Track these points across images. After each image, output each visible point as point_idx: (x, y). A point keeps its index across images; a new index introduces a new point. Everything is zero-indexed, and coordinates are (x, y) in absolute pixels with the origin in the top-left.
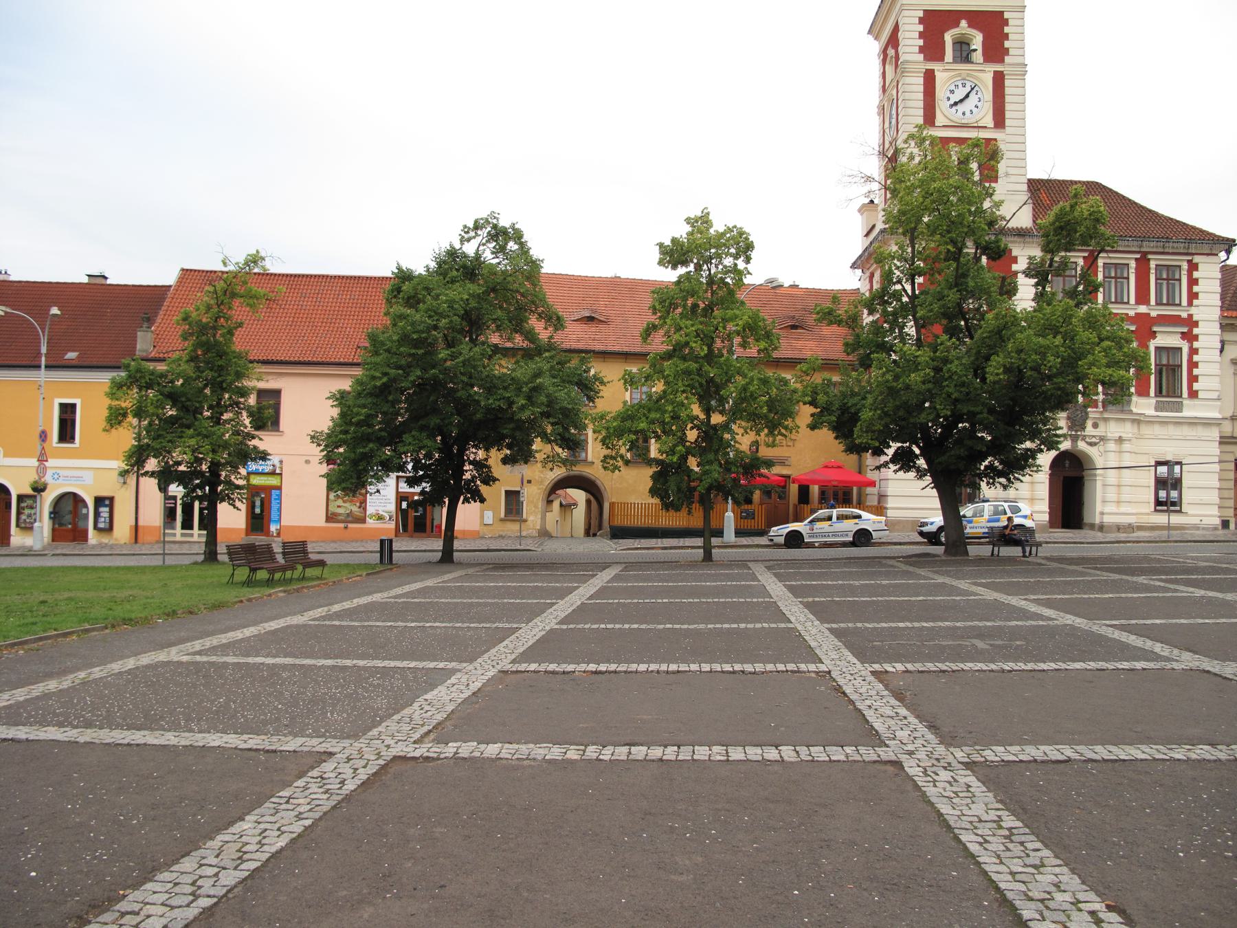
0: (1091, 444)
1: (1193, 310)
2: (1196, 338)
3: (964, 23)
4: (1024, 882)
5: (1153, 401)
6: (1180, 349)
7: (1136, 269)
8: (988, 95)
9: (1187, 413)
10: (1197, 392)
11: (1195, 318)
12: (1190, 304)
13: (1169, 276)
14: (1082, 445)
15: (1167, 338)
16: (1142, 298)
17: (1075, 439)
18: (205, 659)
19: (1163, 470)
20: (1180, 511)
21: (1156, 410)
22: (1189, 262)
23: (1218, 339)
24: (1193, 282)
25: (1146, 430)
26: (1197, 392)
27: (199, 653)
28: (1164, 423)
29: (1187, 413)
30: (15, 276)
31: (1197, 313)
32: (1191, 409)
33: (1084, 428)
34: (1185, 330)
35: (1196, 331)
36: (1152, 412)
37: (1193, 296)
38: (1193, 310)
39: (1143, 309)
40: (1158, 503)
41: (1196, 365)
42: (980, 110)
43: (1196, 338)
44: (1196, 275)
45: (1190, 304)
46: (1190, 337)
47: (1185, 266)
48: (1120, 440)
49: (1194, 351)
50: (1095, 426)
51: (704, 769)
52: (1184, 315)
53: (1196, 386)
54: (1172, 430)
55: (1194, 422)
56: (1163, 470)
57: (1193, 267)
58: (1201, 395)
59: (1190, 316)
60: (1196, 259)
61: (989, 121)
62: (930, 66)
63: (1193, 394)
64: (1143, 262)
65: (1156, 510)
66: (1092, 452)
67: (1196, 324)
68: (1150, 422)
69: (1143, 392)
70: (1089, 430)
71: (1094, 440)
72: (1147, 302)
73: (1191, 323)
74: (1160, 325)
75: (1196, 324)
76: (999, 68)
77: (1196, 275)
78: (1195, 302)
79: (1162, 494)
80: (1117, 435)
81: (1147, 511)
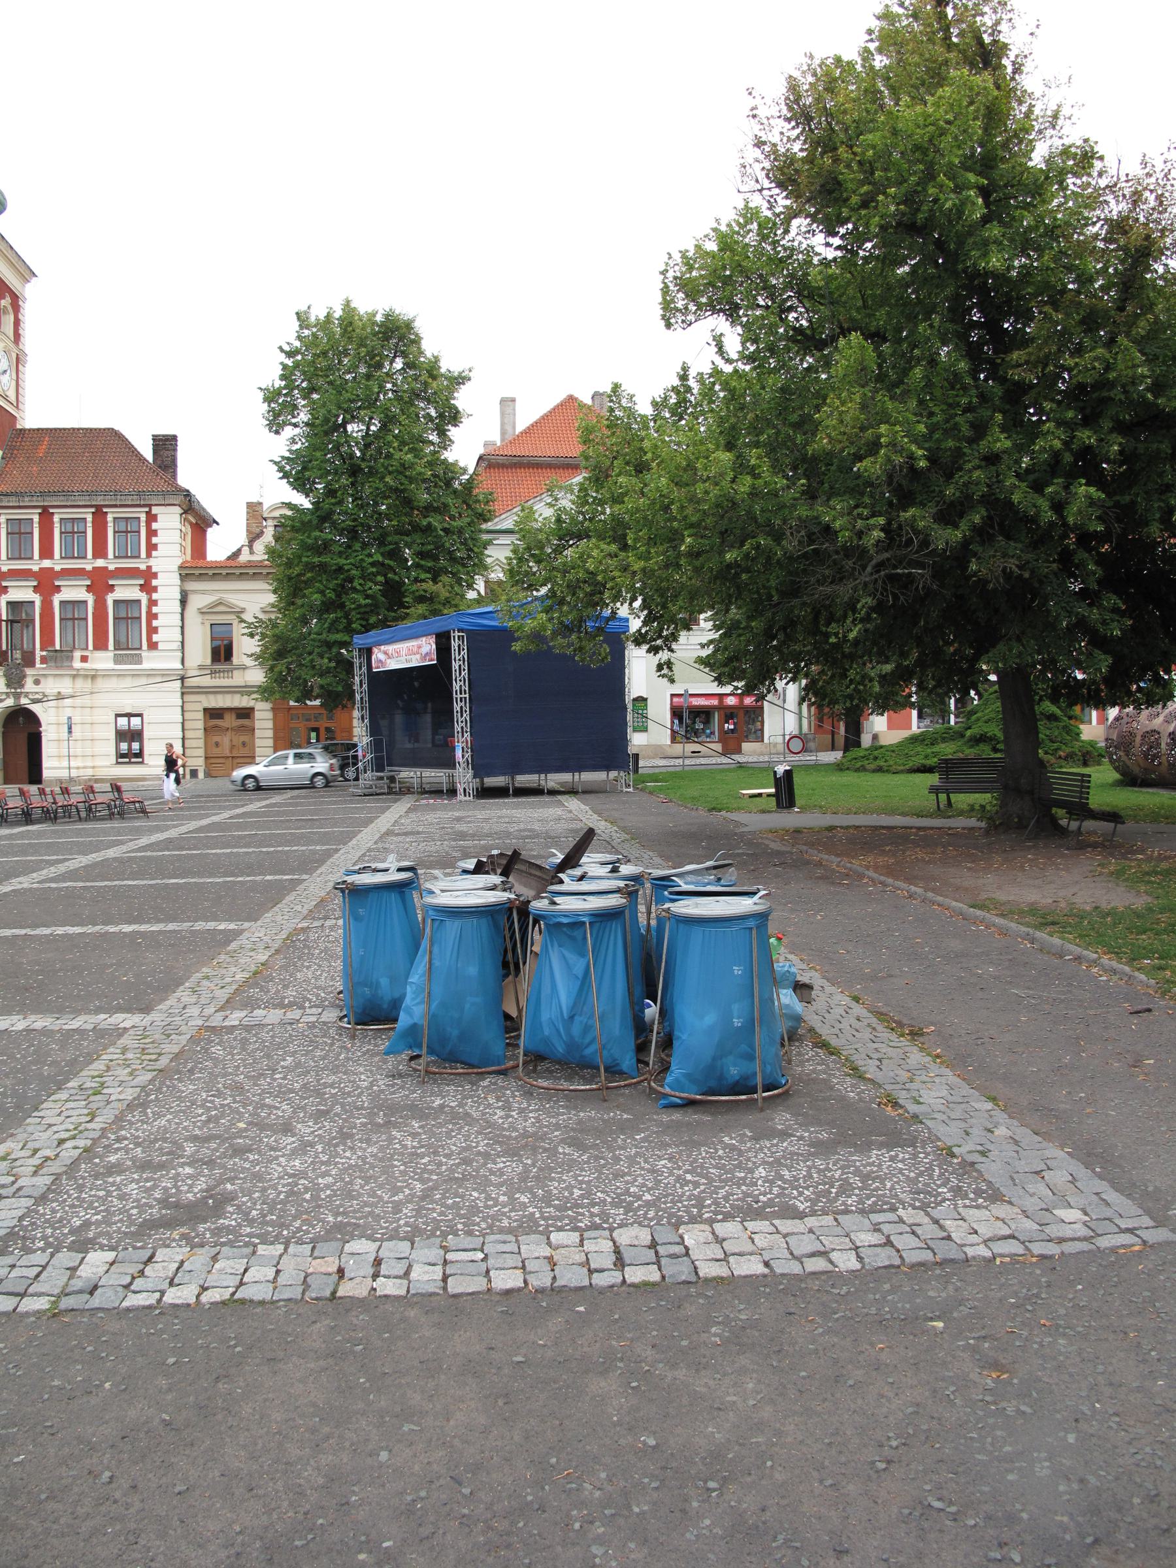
1: (152, 562)
2: (155, 589)
5: (111, 654)
6: (85, 602)
7: (93, 522)
9: (146, 665)
10: (156, 643)
11: (154, 570)
12: (149, 555)
13: (127, 530)
14: (24, 701)
15: (127, 591)
18: (53, 885)
19: (123, 722)
20: (142, 763)
21: (116, 662)
22: (148, 513)
23: (178, 589)
24: (152, 533)
26: (156, 643)
27: (52, 880)
29: (146, 665)
31: (156, 564)
32: (151, 661)
33: (22, 686)
34: (142, 582)
35: (154, 583)
36: (111, 665)
37: (151, 548)
38: (152, 562)
41: (155, 616)
43: (155, 589)
44: (154, 526)
45: (149, 555)
46: (148, 588)
47: (143, 517)
50: (37, 682)
51: (184, 1008)
52: (143, 567)
53: (155, 638)
54: (128, 682)
55: (150, 674)
56: (123, 722)
57: (151, 518)
58: (160, 646)
59: (149, 568)
60: (155, 510)
63: (153, 646)
64: (99, 515)
65: (118, 763)
67: (155, 576)
68: (107, 675)
69: (100, 645)
70: (29, 686)
71: (37, 696)
74: (117, 578)
75: (155, 576)
77: (154, 526)
78: (154, 553)
79: (124, 746)
80: (56, 691)
81: (108, 764)
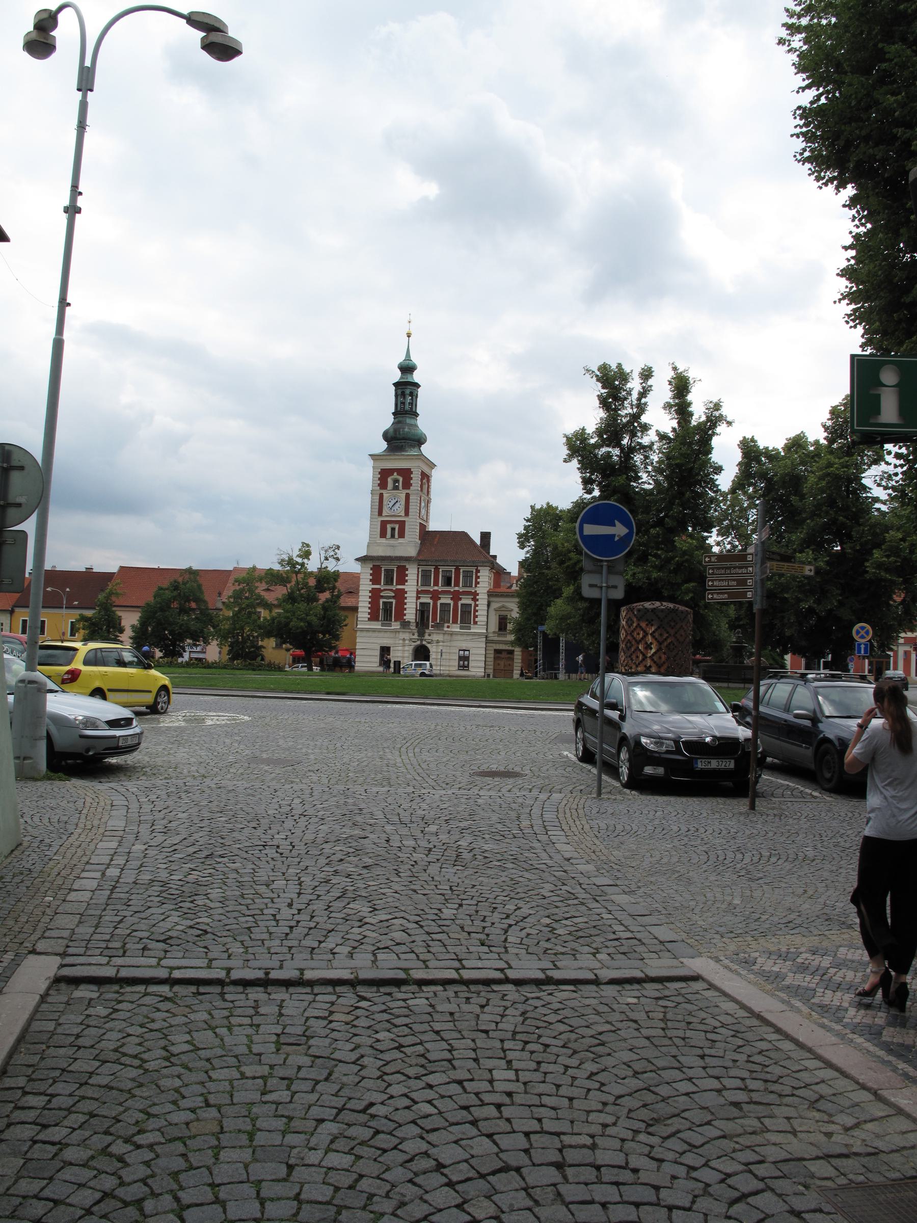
0: (429, 643)
1: (477, 589)
3: (395, 474)
4: (717, 1078)
8: (403, 502)
13: (468, 575)
14: (424, 643)
15: (466, 600)
16: (436, 584)
17: (422, 640)
25: (455, 637)
28: (462, 634)
30: (847, 391)
31: (479, 590)
37: (477, 583)
38: (477, 589)
39: (436, 588)
40: (459, 666)
42: (400, 509)
46: (475, 600)
48: (438, 642)
49: (476, 605)
54: (465, 637)
55: (475, 634)
56: (462, 653)
57: (478, 571)
61: (403, 514)
62: (382, 491)
63: (475, 623)
64: (437, 569)
66: (428, 646)
67: (478, 594)
70: (427, 637)
72: (380, 584)
73: (476, 594)
76: (407, 491)
79: (461, 663)
